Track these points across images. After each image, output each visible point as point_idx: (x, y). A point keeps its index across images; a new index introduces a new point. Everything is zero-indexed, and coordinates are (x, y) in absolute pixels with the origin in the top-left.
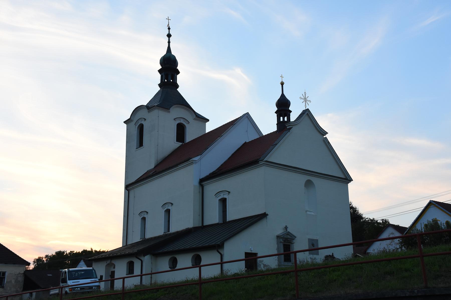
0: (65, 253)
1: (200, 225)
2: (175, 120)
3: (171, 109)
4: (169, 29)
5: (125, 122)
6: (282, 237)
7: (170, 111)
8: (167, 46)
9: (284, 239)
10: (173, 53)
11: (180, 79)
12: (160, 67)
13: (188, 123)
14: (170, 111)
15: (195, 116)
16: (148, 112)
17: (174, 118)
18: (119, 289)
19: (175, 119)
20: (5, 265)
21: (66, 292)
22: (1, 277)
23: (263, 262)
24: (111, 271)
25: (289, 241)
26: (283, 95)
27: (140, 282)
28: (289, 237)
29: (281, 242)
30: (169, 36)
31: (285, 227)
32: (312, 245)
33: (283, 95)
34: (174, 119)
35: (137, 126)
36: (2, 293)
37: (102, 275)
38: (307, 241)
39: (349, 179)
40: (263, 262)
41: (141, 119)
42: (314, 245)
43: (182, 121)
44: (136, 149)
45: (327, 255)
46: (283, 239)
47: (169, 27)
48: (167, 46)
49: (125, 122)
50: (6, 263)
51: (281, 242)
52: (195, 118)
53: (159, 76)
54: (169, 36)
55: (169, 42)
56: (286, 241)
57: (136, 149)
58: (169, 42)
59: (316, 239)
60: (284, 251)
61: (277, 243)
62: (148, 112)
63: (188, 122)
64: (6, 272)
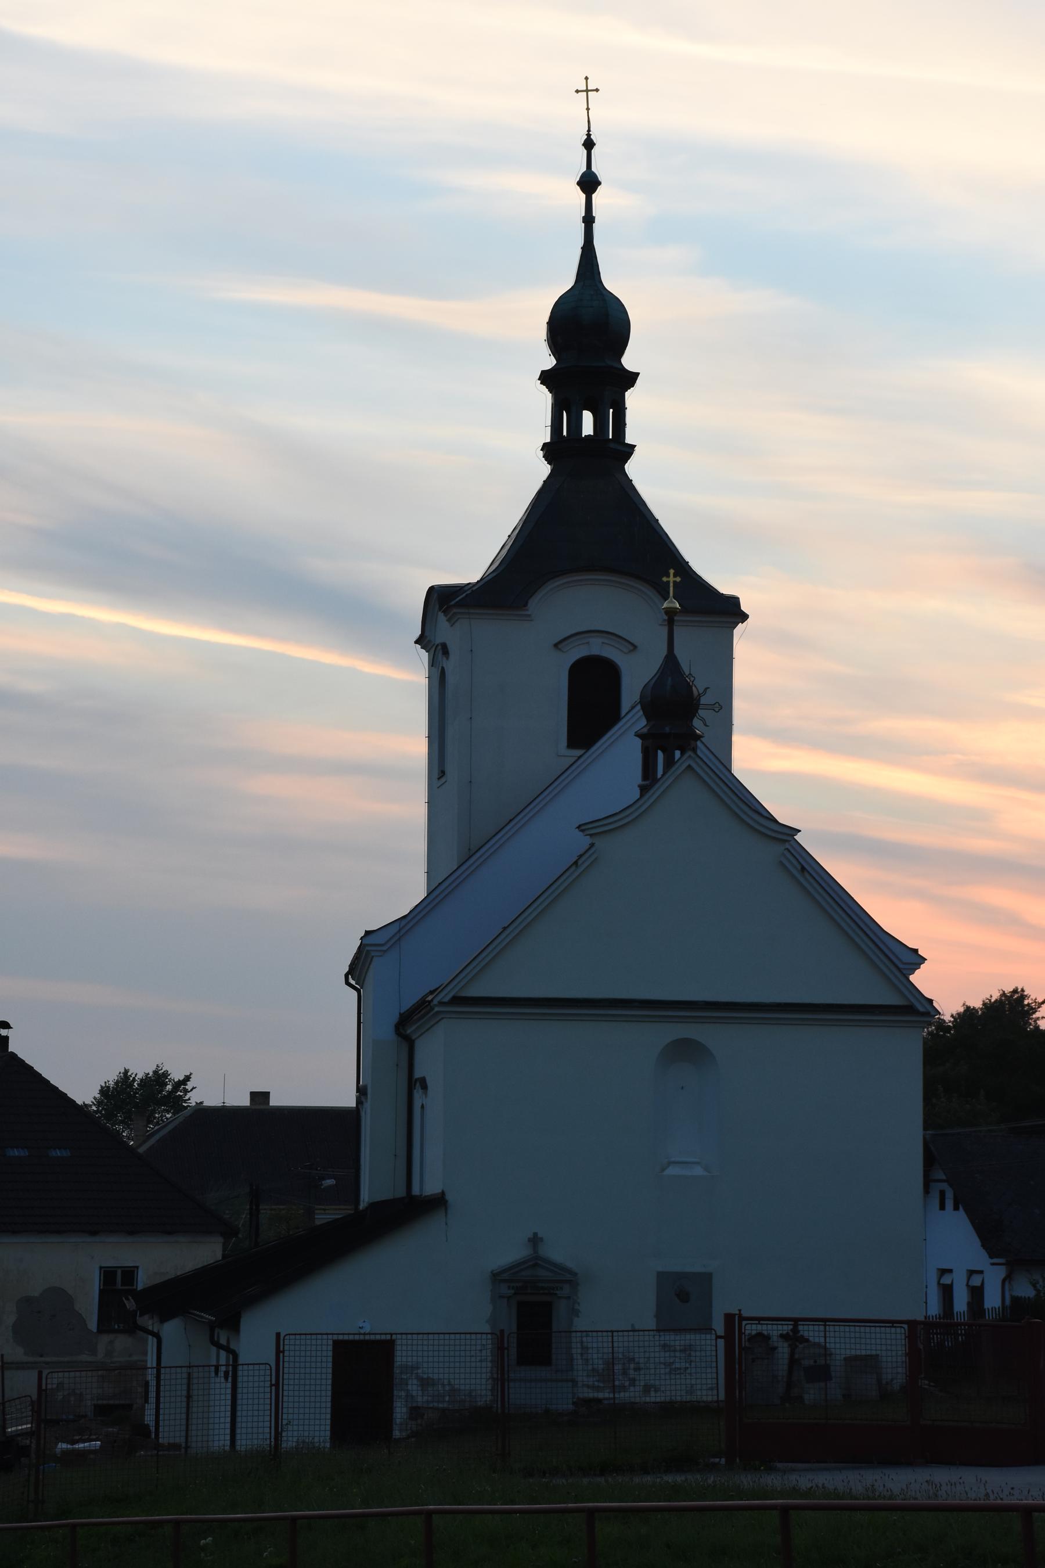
0: (978, 1012)
1: (401, 1193)
2: (560, 650)
5: (416, 642)
7: (529, 616)
13: (631, 648)
31: (529, 1240)
33: (671, 662)
34: (556, 645)
37: (278, 1331)
39: (921, 1009)
40: (420, 1371)
43: (596, 648)
44: (439, 779)
48: (580, 242)
49: (416, 642)
53: (544, 398)
57: (439, 779)
63: (626, 644)
64: (137, 1267)
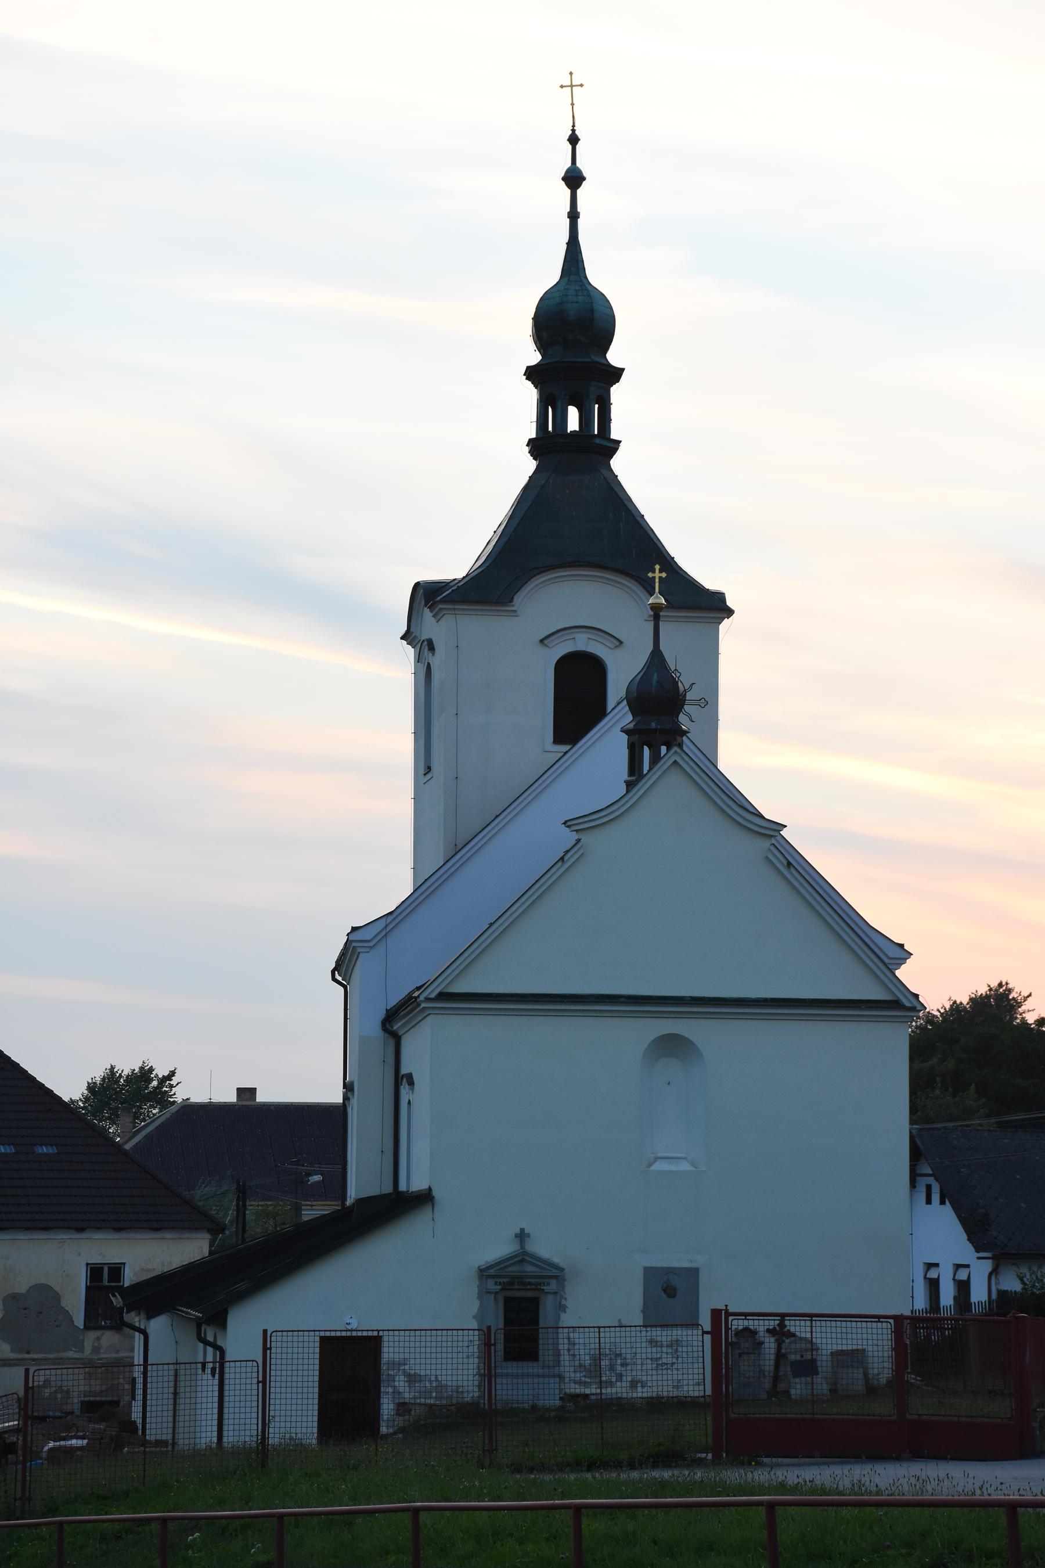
1: (388, 1189)
4: (574, 140)
5: (402, 638)
6: (492, 1272)
7: (515, 611)
8: (566, 238)
9: (506, 1280)
10: (597, 275)
12: (535, 358)
13: (617, 643)
16: (434, 616)
19: (546, 642)
20: (116, 1235)
22: (107, 1284)
23: (407, 1367)
25: (530, 1284)
26: (657, 657)
27: (989, 1260)
28: (529, 1269)
29: (489, 1293)
30: (574, 179)
31: (516, 1236)
32: (665, 1291)
33: (657, 657)
34: (542, 641)
36: (117, 1352)
38: (639, 1275)
39: (908, 1004)
40: (407, 1367)
42: (675, 1289)
43: (582, 643)
45: (952, 1297)
46: (499, 1280)
49: (402, 638)
50: (118, 1230)
51: (489, 1293)
54: (574, 179)
56: (516, 1287)
59: (685, 1264)
60: (505, 1325)
61: (480, 1296)
64: (124, 1264)
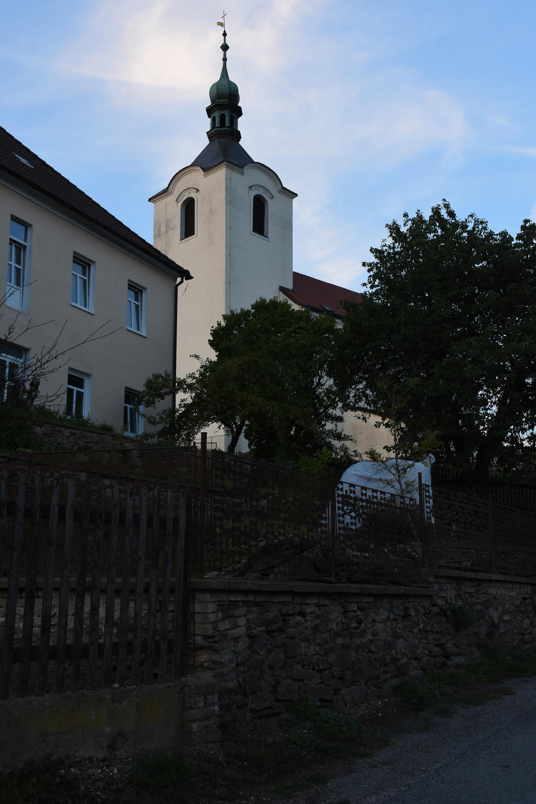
3: (246, 168)
7: (244, 173)
11: (242, 124)
13: (272, 197)
14: (244, 173)
15: (280, 187)
17: (249, 186)
18: (156, 443)
19: (252, 188)
21: (385, 701)
24: (125, 403)
35: (180, 204)
41: (189, 189)
43: (261, 192)
47: (225, 31)
52: (280, 190)
54: (225, 48)
55: (225, 60)
57: (181, 240)
58: (225, 60)
62: (203, 176)
